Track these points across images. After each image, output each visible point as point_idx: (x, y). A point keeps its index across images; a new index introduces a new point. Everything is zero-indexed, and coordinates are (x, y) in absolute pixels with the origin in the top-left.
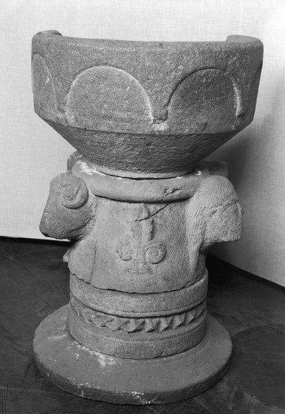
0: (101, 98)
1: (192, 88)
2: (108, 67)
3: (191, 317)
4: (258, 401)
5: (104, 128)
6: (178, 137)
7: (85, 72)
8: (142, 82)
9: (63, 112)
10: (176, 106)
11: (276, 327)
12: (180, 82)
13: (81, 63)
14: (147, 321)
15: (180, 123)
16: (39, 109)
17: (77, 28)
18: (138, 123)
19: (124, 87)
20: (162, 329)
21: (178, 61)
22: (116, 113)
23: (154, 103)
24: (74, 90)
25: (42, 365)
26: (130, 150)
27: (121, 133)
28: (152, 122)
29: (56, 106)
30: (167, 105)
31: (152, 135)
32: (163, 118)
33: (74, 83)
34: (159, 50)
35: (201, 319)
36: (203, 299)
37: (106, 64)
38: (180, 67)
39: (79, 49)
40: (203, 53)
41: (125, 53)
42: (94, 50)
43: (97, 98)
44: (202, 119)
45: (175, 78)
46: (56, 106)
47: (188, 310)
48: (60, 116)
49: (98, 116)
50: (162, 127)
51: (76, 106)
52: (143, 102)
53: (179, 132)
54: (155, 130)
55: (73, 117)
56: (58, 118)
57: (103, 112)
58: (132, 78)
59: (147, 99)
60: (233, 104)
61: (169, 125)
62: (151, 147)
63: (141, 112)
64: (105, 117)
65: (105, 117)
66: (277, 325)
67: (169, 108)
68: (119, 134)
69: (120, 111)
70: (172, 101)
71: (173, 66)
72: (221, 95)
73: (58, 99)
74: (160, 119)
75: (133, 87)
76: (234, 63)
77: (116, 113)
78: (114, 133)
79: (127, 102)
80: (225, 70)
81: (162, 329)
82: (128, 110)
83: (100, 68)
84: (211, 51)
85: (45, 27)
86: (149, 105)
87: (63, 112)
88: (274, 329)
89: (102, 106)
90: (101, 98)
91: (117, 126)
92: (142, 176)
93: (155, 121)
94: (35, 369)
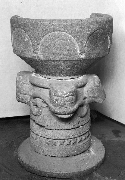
0: (56, 46)
1: (94, 38)
2: (59, 32)
3: (84, 137)
4: (99, 176)
5: (58, 59)
6: (88, 60)
7: (48, 35)
8: (75, 37)
9: (37, 53)
10: (88, 47)
11: (107, 142)
12: (90, 36)
13: (46, 31)
14: (78, 138)
15: (90, 54)
16: (15, 51)
17: (24, 15)
18: (73, 55)
19: (67, 40)
20: (78, 142)
21: (89, 27)
22: (64, 52)
23: (80, 46)
24: (42, 43)
25: (25, 164)
26: (67, 67)
27: (66, 61)
28: (79, 54)
29: (32, 51)
30: (85, 46)
31: (79, 60)
32: (83, 53)
33: (42, 40)
34: (81, 23)
35: (89, 138)
36: (89, 129)
37: (58, 31)
38: (90, 30)
39: (44, 24)
40: (98, 23)
41: (67, 25)
42: (52, 25)
43: (54, 46)
44: (98, 51)
45: (88, 34)
46: (32, 51)
47: (82, 135)
48: (35, 55)
49: (55, 54)
50: (83, 56)
51: (43, 50)
52: (75, 46)
53: (90, 58)
54: (80, 58)
55: (42, 55)
56: (33, 56)
57: (57, 52)
58: (70, 36)
59: (77, 45)
60: (108, 43)
61: (86, 55)
62: (76, 65)
63: (74, 50)
64: (58, 54)
65: (58, 54)
66: (107, 141)
67: (86, 48)
68: (64, 61)
69: (65, 51)
70: (87, 44)
71: (87, 29)
72: (104, 40)
73: (33, 48)
74: (82, 53)
75: (71, 40)
76: (108, 26)
77: (64, 52)
78: (62, 61)
79: (68, 46)
80: (105, 30)
81: (78, 142)
82: (69, 50)
83: (55, 33)
84: (101, 22)
85: (15, 14)
86: (78, 47)
87: (37, 53)
88: (106, 143)
89: (56, 49)
90: (56, 46)
91: (64, 57)
92: (68, 78)
93: (80, 54)
94: (22, 166)
